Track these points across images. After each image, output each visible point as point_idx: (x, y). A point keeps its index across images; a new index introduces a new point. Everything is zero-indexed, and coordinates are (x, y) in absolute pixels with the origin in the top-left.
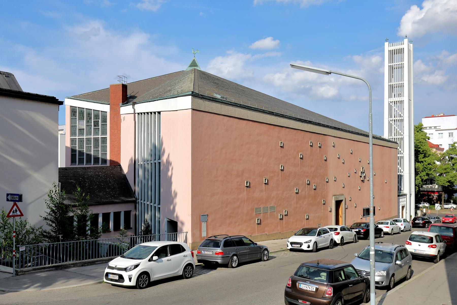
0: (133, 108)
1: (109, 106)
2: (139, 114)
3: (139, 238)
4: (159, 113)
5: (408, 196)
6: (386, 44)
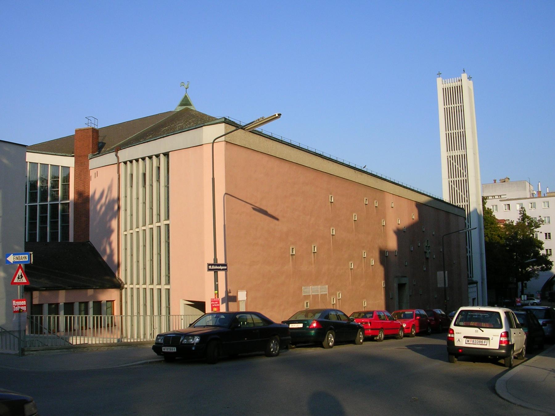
0: (116, 155)
1: (74, 158)
2: (125, 163)
3: (127, 337)
4: (166, 155)
5: (479, 284)
6: (439, 80)
